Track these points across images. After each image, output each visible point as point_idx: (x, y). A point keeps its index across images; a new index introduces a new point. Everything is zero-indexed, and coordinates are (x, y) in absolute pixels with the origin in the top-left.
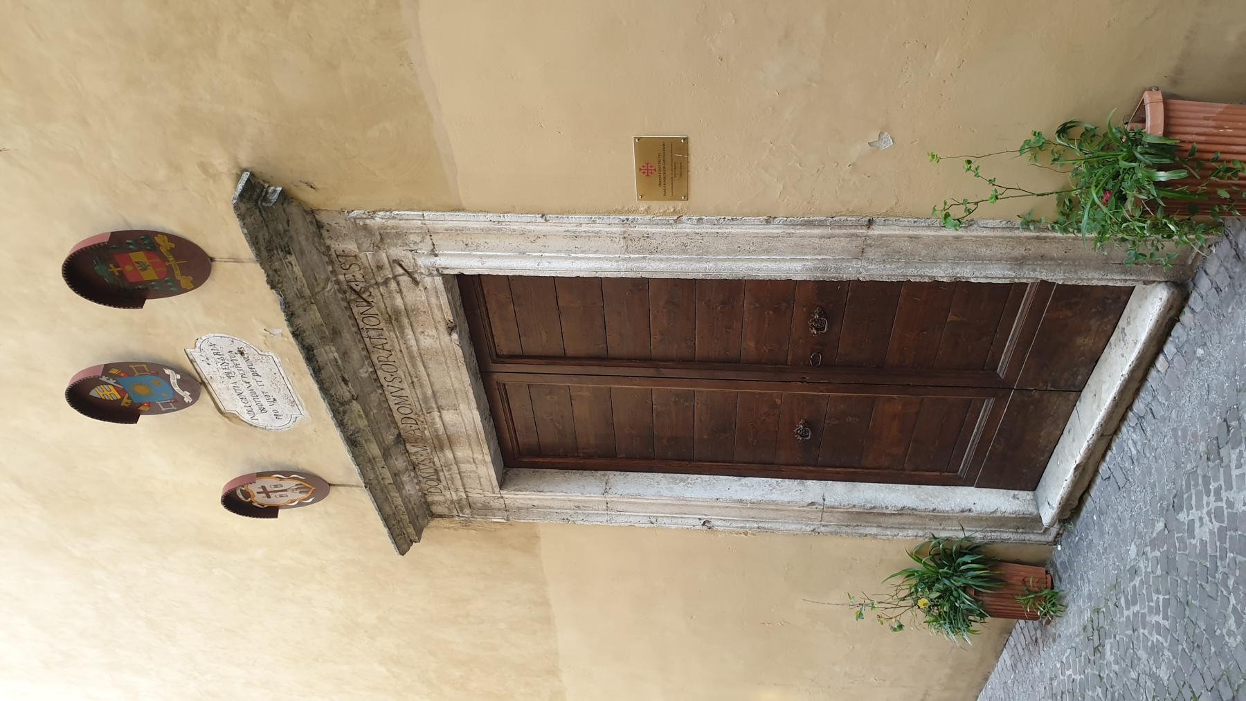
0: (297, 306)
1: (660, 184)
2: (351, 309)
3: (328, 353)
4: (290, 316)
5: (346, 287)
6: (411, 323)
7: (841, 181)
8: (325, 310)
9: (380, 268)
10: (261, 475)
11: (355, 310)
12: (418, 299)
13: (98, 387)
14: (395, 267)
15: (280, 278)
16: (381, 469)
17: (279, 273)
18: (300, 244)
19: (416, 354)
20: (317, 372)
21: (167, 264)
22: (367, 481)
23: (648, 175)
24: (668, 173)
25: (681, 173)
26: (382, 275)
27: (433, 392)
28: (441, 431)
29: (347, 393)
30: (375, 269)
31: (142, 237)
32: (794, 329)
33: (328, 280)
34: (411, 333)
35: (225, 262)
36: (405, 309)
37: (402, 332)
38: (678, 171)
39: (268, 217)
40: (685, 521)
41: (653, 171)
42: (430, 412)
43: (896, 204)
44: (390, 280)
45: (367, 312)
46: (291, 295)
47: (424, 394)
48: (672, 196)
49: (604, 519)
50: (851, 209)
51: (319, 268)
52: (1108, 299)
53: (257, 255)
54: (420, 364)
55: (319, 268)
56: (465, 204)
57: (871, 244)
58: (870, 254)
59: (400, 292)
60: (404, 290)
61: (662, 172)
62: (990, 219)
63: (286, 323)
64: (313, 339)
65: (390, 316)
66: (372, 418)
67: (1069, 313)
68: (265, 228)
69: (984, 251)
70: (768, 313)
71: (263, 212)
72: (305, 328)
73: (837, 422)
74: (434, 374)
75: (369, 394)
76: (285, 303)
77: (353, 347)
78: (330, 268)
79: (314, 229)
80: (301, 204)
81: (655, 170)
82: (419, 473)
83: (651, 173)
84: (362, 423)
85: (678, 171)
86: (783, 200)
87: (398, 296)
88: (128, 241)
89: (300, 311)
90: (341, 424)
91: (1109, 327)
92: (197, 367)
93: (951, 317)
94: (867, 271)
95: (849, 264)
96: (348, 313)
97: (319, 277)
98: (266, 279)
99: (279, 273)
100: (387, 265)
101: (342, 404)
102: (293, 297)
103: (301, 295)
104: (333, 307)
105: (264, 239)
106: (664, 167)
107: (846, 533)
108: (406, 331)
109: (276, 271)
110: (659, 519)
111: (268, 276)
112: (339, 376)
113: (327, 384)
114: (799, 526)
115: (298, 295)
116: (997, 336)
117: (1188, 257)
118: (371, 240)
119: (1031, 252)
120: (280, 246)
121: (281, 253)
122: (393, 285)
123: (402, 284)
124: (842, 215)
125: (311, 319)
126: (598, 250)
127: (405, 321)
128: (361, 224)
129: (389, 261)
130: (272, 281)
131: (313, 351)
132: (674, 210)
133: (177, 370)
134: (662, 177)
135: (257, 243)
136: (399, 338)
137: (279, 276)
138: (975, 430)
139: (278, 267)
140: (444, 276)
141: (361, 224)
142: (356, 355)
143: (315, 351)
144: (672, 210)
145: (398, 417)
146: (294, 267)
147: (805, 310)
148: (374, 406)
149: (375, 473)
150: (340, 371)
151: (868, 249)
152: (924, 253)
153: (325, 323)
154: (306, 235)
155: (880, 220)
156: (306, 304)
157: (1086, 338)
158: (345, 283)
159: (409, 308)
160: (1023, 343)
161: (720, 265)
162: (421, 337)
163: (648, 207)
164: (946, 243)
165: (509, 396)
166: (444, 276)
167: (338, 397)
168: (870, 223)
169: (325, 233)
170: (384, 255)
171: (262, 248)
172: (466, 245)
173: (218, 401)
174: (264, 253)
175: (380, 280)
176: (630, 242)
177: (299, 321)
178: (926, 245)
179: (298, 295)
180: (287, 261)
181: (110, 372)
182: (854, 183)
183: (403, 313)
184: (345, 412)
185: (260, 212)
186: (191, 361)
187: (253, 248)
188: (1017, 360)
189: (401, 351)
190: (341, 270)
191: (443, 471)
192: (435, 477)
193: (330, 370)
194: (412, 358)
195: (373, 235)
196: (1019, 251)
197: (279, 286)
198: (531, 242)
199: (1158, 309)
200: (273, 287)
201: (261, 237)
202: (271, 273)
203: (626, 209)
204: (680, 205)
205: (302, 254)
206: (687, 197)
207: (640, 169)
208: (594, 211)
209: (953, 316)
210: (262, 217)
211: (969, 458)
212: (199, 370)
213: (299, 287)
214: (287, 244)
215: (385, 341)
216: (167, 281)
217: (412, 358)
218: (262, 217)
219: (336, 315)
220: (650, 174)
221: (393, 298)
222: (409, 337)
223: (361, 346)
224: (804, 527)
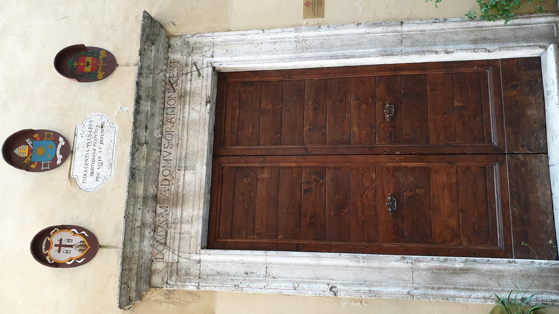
0: (144, 72)
1: (312, 10)
2: (165, 94)
3: (146, 106)
4: (140, 74)
5: (168, 81)
6: (190, 101)
7: (386, 4)
8: (155, 82)
9: (187, 65)
10: (63, 228)
11: (167, 95)
12: (198, 85)
13: (20, 156)
14: (193, 67)
15: (144, 53)
16: (138, 209)
17: (145, 51)
18: (159, 46)
19: (186, 124)
20: (137, 112)
21: (98, 64)
22: (127, 213)
23: (308, 7)
24: (316, 5)
25: (321, 4)
26: (186, 70)
27: (186, 154)
28: (180, 190)
29: (144, 138)
30: (184, 65)
31: (96, 50)
32: (377, 117)
33: (162, 71)
34: (188, 107)
35: (122, 66)
36: (190, 91)
37: (184, 106)
38: (320, 4)
39: (153, 25)
40: (318, 286)
41: (310, 5)
42: (180, 170)
43: (411, 13)
44: (188, 73)
45: (172, 96)
46: (145, 64)
47: (181, 154)
48: (317, 16)
49: (262, 285)
50: (392, 17)
51: (161, 62)
52: (532, 81)
53: (142, 35)
54: (185, 130)
55: (161, 62)
56: (232, 28)
57: (404, 37)
58: (405, 42)
59: (191, 80)
60: (193, 80)
61: (314, 5)
62: (453, 18)
63: (137, 75)
64: (143, 94)
65: (181, 95)
66: (148, 167)
67: (515, 93)
68: (150, 29)
69: (455, 37)
70: (363, 106)
71: (152, 22)
72: (143, 85)
73: (411, 194)
74: (190, 139)
75: (153, 150)
76: (141, 66)
77: (158, 114)
78: (165, 67)
79: (167, 45)
80: (166, 31)
81: (311, 4)
82: (156, 236)
83: (309, 3)
84: (143, 164)
85: (320, 4)
86: (364, 15)
87: (189, 83)
88: (89, 51)
89: (145, 75)
90: (133, 155)
91: (540, 100)
92: (75, 139)
93: (456, 104)
94: (405, 50)
95: (397, 48)
96: (163, 95)
97: (159, 67)
98: (139, 49)
99: (145, 51)
100: (190, 65)
101: (139, 143)
102: (145, 66)
103: (148, 68)
104: (159, 85)
105: (147, 33)
106: (314, 2)
107: (433, 295)
108: (186, 106)
109: (145, 49)
110: (300, 285)
111: (141, 49)
112: (145, 124)
113: (138, 124)
114: (398, 289)
115: (148, 67)
116: (484, 115)
117: (553, 33)
118: (188, 50)
119: (478, 36)
120: (151, 40)
121: (150, 44)
122: (189, 75)
123: (193, 76)
124: (389, 21)
125: (147, 83)
126: (283, 50)
127: (188, 98)
128: (187, 40)
129: (192, 62)
130: (141, 52)
131: (140, 100)
132: (318, 23)
133: (65, 140)
134: (313, 7)
135: (144, 32)
136: (182, 109)
137: (145, 52)
138: (496, 196)
139: (146, 48)
140: (214, 68)
141: (187, 40)
142: (157, 120)
143: (141, 101)
144: (317, 23)
145: (161, 178)
146: (152, 52)
147: (381, 103)
148: (152, 160)
149: (134, 210)
150: (147, 120)
151: (404, 40)
152: (429, 41)
153: (152, 88)
154: (163, 44)
155: (406, 22)
156: (149, 74)
157: (531, 110)
158: (168, 79)
159: (192, 92)
160: (499, 117)
161: (338, 52)
162: (191, 112)
163: (307, 22)
164: (438, 34)
165: (223, 182)
166: (214, 68)
167: (139, 137)
168: (402, 23)
169: (170, 50)
170: (191, 58)
171: (145, 36)
172: (227, 51)
173: (72, 167)
174: (144, 38)
175: (184, 72)
176: (298, 43)
177: (142, 80)
178: (429, 36)
179: (148, 67)
180: (151, 48)
181: (33, 136)
182: (392, 4)
183: (188, 94)
184: (138, 150)
185: (151, 22)
186: (75, 135)
187: (142, 32)
188: (500, 130)
189: (179, 119)
190: (169, 70)
191: (171, 229)
192: (163, 241)
193: (142, 117)
194: (183, 125)
195: (189, 47)
196: (472, 37)
197: (143, 56)
198: (255, 47)
199: (553, 55)
200: (140, 55)
201: (146, 31)
202: (142, 48)
203: (298, 24)
204: (320, 20)
205: (157, 52)
206: (323, 17)
207: (305, 4)
208: (284, 27)
209: (457, 103)
210: (151, 24)
211: (501, 235)
212: (75, 142)
213: (149, 64)
214: (155, 39)
215: (173, 116)
216: (93, 76)
217: (183, 125)
218: (151, 24)
219: (158, 90)
220: (310, 3)
221: (186, 84)
222: (186, 110)
223: (162, 101)
224: (401, 290)
